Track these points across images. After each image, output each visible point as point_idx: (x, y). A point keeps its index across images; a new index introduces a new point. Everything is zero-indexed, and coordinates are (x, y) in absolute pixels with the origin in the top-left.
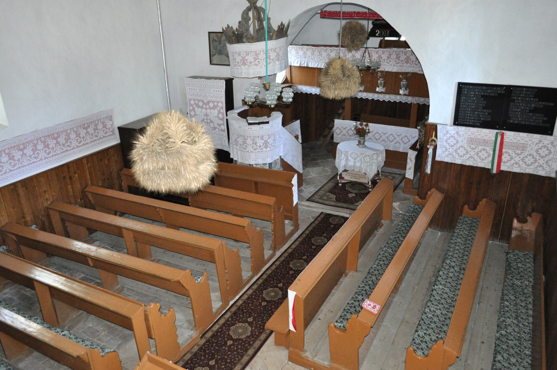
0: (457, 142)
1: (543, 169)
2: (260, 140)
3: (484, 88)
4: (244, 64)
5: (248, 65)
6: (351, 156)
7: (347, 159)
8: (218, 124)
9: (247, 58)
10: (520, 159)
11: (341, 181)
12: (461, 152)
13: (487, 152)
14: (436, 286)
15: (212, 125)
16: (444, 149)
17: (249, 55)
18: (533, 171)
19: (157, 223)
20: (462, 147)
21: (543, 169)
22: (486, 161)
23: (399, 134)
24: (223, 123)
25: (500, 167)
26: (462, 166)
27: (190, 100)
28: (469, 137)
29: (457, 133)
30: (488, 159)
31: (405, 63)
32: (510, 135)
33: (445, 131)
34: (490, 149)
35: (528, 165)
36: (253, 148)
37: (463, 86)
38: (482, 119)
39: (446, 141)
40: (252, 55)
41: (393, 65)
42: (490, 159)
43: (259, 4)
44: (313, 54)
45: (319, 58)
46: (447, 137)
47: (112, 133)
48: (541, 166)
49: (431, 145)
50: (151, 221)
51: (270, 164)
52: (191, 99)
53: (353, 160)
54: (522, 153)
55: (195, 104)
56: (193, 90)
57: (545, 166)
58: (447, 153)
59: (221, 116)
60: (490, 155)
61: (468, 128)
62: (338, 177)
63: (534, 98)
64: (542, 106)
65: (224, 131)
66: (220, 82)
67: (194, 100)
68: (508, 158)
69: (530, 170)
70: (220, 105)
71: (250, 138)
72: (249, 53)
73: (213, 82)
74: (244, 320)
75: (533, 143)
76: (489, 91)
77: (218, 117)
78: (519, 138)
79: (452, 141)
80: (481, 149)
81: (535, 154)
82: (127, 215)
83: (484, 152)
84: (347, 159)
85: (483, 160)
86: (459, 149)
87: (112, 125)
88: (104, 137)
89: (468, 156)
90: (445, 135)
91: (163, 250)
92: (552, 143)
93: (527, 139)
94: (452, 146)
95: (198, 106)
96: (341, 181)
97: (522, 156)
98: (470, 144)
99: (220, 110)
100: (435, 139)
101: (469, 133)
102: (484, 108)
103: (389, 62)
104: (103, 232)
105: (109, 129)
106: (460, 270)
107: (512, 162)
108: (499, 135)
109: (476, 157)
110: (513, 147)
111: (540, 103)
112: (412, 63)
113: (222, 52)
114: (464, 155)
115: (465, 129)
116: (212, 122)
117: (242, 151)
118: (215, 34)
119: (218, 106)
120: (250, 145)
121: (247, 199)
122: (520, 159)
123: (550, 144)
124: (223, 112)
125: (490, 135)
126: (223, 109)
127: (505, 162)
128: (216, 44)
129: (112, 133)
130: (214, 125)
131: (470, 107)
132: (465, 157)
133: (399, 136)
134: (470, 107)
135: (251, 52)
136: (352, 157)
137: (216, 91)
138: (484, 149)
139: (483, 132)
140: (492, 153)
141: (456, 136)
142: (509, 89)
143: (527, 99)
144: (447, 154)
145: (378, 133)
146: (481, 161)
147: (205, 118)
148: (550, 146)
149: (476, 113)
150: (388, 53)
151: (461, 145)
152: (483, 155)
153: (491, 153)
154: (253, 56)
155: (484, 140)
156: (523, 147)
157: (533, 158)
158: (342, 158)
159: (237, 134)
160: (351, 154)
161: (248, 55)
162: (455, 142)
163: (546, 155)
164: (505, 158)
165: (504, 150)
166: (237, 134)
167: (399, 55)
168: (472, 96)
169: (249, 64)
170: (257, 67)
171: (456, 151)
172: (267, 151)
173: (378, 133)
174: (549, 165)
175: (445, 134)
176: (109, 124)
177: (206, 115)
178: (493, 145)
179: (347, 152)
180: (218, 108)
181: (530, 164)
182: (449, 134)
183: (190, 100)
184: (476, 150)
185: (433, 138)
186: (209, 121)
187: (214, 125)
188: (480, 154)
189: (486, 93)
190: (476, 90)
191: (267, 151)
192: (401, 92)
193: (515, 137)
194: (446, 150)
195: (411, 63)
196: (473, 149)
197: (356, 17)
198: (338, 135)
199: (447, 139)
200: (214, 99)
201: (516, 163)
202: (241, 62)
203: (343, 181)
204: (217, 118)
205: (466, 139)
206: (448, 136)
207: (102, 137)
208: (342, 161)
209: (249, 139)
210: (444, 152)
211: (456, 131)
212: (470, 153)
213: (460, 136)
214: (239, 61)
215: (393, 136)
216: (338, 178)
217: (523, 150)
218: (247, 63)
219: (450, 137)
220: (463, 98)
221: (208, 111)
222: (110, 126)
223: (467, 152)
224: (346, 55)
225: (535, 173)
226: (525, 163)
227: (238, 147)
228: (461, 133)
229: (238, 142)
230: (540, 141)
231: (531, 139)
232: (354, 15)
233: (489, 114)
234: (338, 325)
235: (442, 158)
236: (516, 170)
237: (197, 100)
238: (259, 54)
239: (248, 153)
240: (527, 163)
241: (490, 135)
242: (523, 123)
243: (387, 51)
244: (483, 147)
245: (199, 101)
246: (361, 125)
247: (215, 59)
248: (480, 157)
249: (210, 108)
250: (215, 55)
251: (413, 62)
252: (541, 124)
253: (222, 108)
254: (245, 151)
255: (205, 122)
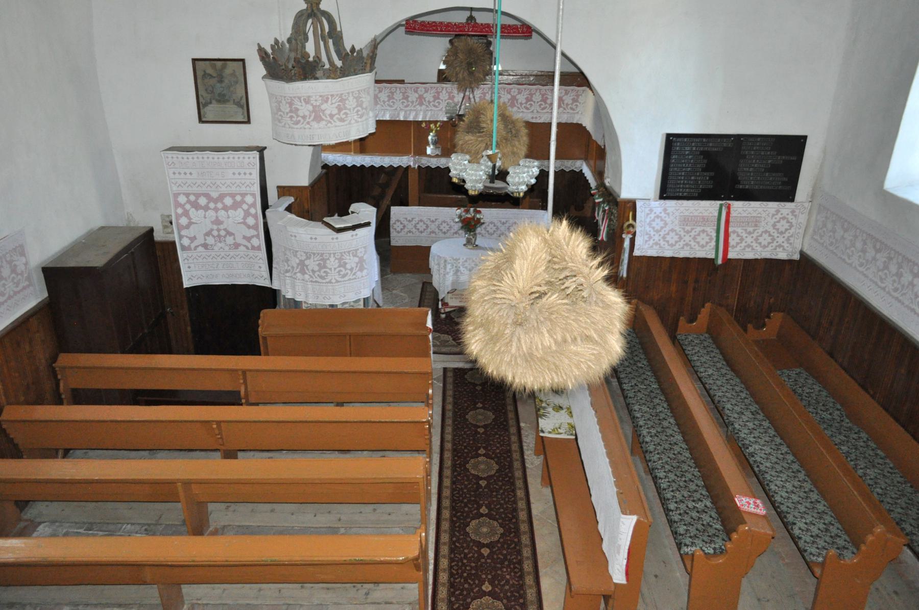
0: (666, 224)
1: (784, 249)
2: (352, 258)
3: (704, 140)
4: (318, 119)
5: (326, 121)
6: (463, 265)
7: (457, 271)
8: (244, 237)
9: (323, 107)
10: (752, 240)
11: (444, 310)
12: (672, 238)
13: (708, 235)
14: (750, 448)
15: (230, 240)
16: (646, 238)
17: (329, 102)
18: (771, 254)
19: (161, 454)
20: (672, 230)
21: (784, 249)
22: (708, 248)
23: (504, 220)
24: (255, 233)
25: (727, 255)
26: (672, 258)
27: (176, 195)
28: (682, 214)
29: (665, 210)
30: (710, 244)
31: (418, 104)
32: (738, 207)
33: (649, 209)
34: (712, 230)
35: (765, 247)
36: (339, 275)
37: (674, 139)
38: (701, 187)
39: (650, 224)
40: (334, 101)
41: (535, 111)
42: (713, 243)
43: (323, 6)
44: (391, 97)
45: (403, 102)
46: (650, 218)
47: (27, 283)
48: (780, 246)
49: (628, 233)
50: (146, 453)
51: (366, 300)
52: (179, 194)
53: (468, 272)
54: (754, 230)
55: (189, 202)
56: (182, 172)
57: (786, 245)
58: (651, 242)
59: (251, 221)
60: (713, 239)
61: (680, 202)
62: (440, 303)
63: (771, 151)
64: (782, 161)
65: (259, 248)
66: (246, 157)
67: (187, 195)
68: (737, 239)
69: (766, 253)
70: (249, 199)
71: (334, 256)
72: (328, 98)
73: (231, 156)
74: (477, 591)
75: (768, 215)
76: (711, 145)
77: (244, 223)
78: (750, 210)
79: (658, 224)
80: (700, 232)
81: (771, 230)
82: (78, 452)
83: (703, 235)
84: (457, 271)
85: (703, 246)
86: (668, 234)
87: (26, 264)
88: (16, 293)
89: (682, 243)
90: (647, 216)
91: (223, 506)
92: (793, 212)
93: (760, 210)
94: (657, 231)
95: (196, 206)
96: (444, 310)
97: (755, 235)
98: (684, 225)
99: (248, 209)
100: (634, 223)
101: (682, 209)
102: (704, 170)
103: (529, 106)
104: (51, 501)
105: (22, 274)
106: (753, 414)
107: (743, 244)
108: (724, 208)
109: (692, 243)
110: (743, 222)
111: (779, 157)
112: (521, 106)
113: (227, 97)
114: (676, 242)
115: (676, 204)
116: (229, 233)
117: (316, 282)
118: (208, 62)
119: (243, 202)
120: (335, 269)
121: (325, 369)
122: (752, 240)
123: (790, 214)
124: (256, 213)
125: (711, 209)
126: (256, 209)
127: (733, 247)
128: (212, 82)
129: (27, 283)
130: (234, 239)
131: (684, 169)
132: (677, 246)
133: (504, 223)
134: (684, 169)
135: (332, 96)
136: (466, 268)
137: (245, 174)
138: (703, 231)
139: (769, 206)
140: (715, 234)
141: (663, 215)
142: (739, 139)
143: (763, 153)
144: (682, 246)
145: (421, 221)
146: (700, 248)
147: (215, 227)
148: (790, 217)
149: (693, 178)
150: (528, 92)
151: (671, 228)
152: (703, 239)
153: (714, 235)
154: (337, 104)
155: (703, 218)
156: (756, 222)
157: (770, 235)
158: (448, 270)
159: (305, 252)
160: (463, 262)
161: (326, 102)
162: (661, 224)
163: (786, 230)
164: (733, 240)
165: (731, 229)
166: (305, 252)
167: (452, 93)
168: (687, 152)
169: (329, 119)
170: (343, 124)
171: (664, 238)
172: (362, 277)
173: (421, 221)
174: (791, 244)
175: (648, 214)
176: (20, 262)
177: (218, 222)
178: (716, 223)
179: (457, 260)
180: (245, 207)
181: (766, 244)
182: (653, 213)
183: (176, 195)
184: (693, 234)
185: (631, 221)
186: (223, 233)
187: (234, 239)
188: (699, 239)
189: (706, 148)
190: (693, 144)
191: (362, 277)
192: (429, 151)
193: (745, 209)
194: (650, 238)
195: (519, 106)
196: (688, 232)
197: (472, 31)
198: (398, 232)
199: (650, 221)
200: (234, 189)
201: (780, 246)
202: (310, 116)
203: (448, 310)
204: (243, 226)
205: (678, 218)
206: (652, 216)
207: (12, 293)
208: (447, 276)
209: (332, 259)
210: (646, 241)
211: (662, 208)
212: (778, 239)
213: (668, 214)
214: (307, 113)
215: (495, 226)
216: (440, 306)
217: (756, 226)
218: (324, 117)
219: (655, 217)
220: (674, 157)
221: (222, 213)
222: (23, 268)
223: (680, 238)
224: (454, 97)
225: (773, 257)
226: (760, 243)
227: (307, 277)
228: (670, 210)
229: (307, 266)
230: (778, 211)
231: (765, 209)
232: (469, 29)
233: (711, 178)
234: (691, 550)
235: (644, 250)
236: (749, 255)
237: (194, 194)
238: (346, 100)
239: (329, 284)
240: (763, 244)
241: (711, 209)
242: (757, 187)
243: (525, 89)
244: (702, 228)
245: (198, 196)
246: (467, 211)
247: (211, 111)
248: (698, 243)
249: (226, 208)
250: (211, 103)
251: (384, 102)
252: (780, 187)
253: (253, 205)
254: (324, 281)
255: (214, 236)
